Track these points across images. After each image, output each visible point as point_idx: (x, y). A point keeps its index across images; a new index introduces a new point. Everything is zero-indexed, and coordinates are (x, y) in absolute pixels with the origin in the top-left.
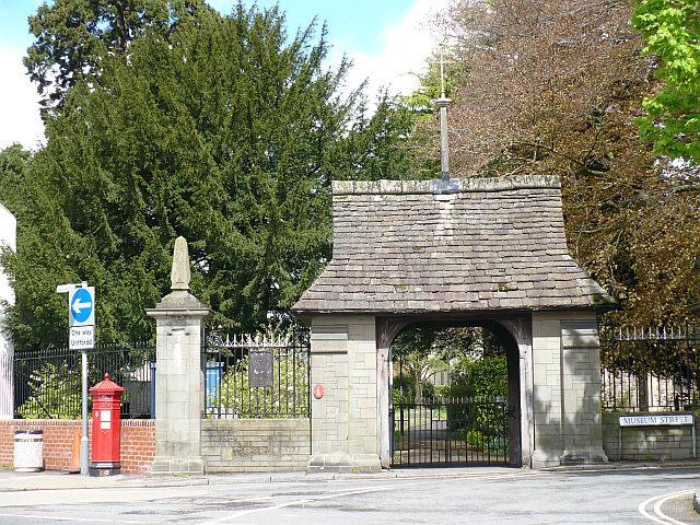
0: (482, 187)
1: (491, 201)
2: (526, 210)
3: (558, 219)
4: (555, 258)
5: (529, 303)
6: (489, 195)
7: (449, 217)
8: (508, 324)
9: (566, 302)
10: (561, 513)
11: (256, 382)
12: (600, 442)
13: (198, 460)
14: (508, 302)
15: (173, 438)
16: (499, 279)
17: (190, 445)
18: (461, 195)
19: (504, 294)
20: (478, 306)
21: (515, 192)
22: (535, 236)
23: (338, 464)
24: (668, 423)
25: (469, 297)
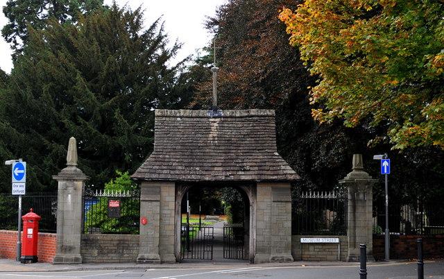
6: (237, 120)
8: (245, 188)
12: (290, 251)
14: (245, 177)
19: (243, 173)
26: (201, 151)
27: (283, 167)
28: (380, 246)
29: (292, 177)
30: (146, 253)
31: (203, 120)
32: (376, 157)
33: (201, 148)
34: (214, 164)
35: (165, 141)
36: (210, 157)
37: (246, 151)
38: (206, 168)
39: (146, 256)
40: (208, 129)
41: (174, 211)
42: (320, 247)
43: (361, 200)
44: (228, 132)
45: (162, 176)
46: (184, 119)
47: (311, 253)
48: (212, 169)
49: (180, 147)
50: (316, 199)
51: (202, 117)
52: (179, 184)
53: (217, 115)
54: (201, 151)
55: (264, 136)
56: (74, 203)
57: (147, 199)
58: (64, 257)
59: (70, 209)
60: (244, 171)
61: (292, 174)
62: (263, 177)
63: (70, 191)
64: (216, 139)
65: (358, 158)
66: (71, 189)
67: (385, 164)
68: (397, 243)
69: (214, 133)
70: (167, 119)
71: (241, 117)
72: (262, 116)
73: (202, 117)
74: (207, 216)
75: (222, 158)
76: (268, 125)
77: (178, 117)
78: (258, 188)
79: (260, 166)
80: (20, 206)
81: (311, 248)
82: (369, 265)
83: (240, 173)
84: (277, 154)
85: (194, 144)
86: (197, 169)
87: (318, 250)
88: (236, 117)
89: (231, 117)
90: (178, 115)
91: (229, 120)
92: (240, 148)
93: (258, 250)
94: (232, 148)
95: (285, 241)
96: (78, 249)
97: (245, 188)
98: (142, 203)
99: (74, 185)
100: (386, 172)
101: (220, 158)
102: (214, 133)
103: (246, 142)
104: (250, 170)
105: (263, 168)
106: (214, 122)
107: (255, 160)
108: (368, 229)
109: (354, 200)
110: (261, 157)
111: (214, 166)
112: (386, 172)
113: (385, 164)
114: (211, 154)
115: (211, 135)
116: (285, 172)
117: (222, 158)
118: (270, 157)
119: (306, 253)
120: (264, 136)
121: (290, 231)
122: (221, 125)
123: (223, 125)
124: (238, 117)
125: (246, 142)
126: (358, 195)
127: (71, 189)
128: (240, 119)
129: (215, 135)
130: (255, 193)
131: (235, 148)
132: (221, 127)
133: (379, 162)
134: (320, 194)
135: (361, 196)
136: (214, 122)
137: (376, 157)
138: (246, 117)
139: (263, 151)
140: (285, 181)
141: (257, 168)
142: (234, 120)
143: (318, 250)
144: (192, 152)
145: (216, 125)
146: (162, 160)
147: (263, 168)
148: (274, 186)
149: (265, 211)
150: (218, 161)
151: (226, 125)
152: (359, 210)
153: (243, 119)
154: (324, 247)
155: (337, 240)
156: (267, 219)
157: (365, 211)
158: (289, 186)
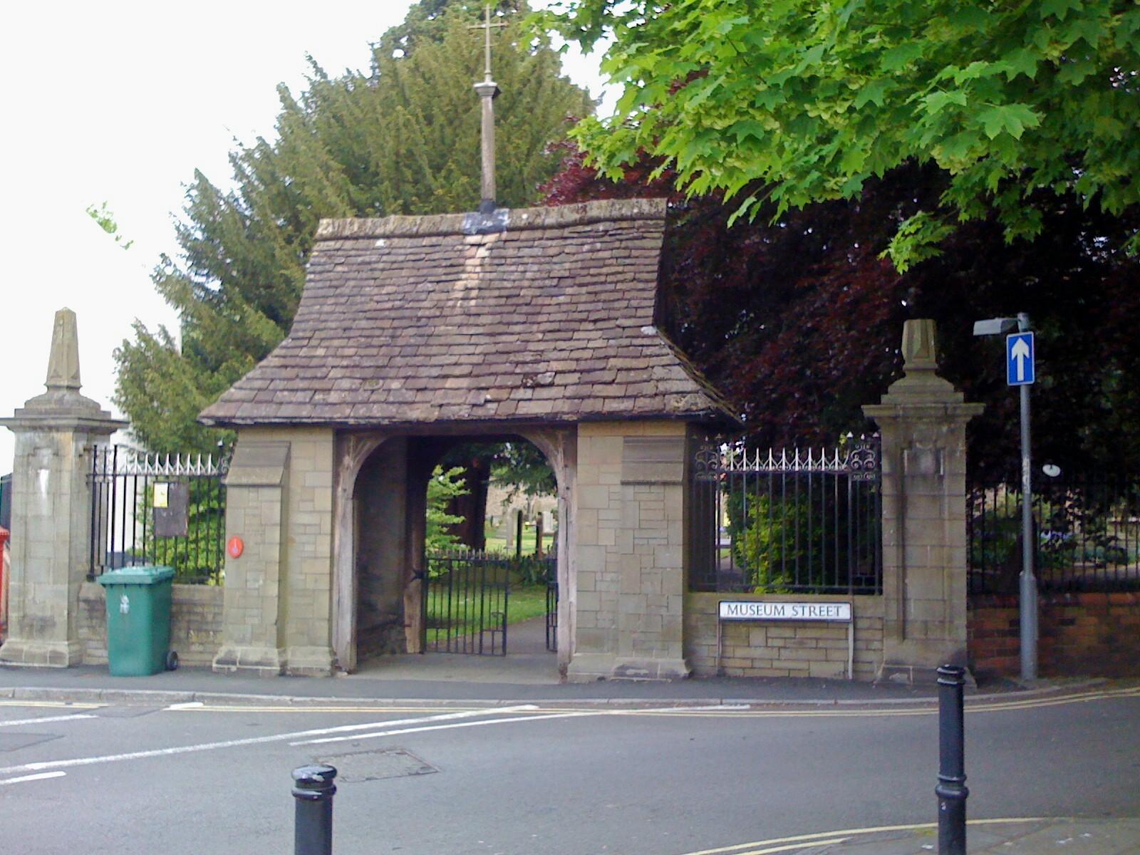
0: (539, 221)
1: (549, 243)
2: (601, 254)
3: (650, 268)
4: (628, 332)
5: (563, 407)
6: (549, 233)
7: (478, 269)
8: (540, 440)
9: (626, 405)
10: (376, 319)
11: (896, 146)
12: (678, 647)
13: (63, 647)
14: (536, 406)
15: (33, 611)
16: (527, 369)
17: (836, 132)
18: (505, 235)
19: (528, 393)
20: (480, 413)
21: (588, 228)
22: (603, 297)
23: (258, 664)
24: (807, 616)
25: (472, 398)
26: (422, 331)
27: (659, 372)
28: (1003, 634)
29: (682, 404)
30: (241, 641)
31: (449, 240)
32: (984, 327)
33: (423, 321)
34: (446, 371)
35: (326, 309)
36: (444, 350)
37: (556, 326)
38: (421, 383)
39: (239, 651)
40: (456, 267)
41: (328, 518)
42: (788, 633)
43: (924, 477)
44: (513, 272)
45: (287, 412)
46: (396, 241)
47: (757, 653)
48: (439, 383)
49: (364, 324)
50: (803, 475)
51: (446, 234)
52: (342, 433)
53: (490, 224)
54: (422, 331)
55: (620, 277)
56: (54, 493)
57: (244, 481)
58: (25, 648)
59: (45, 510)
60: (533, 387)
61: (683, 393)
62: (589, 406)
63: (45, 461)
64: (474, 293)
65: (917, 336)
66: (46, 455)
67: (1020, 350)
68: (1071, 622)
69: (470, 279)
70: (348, 244)
71: (562, 226)
72: (623, 219)
73: (446, 234)
74: (840, 702)
75: (479, 349)
76: (638, 243)
77: (377, 237)
78: (580, 440)
79: (589, 371)
80: (211, 746)
81: (757, 636)
82: (977, 707)
83: (521, 393)
84: (650, 330)
85: (407, 313)
86: (395, 385)
87: (780, 643)
88: (544, 228)
89: (531, 227)
90: (379, 231)
91: (524, 235)
92: (540, 318)
93: (590, 639)
94: (516, 318)
95: (663, 611)
96: (62, 628)
97: (540, 440)
98: (232, 494)
99: (52, 444)
100: (1021, 376)
101: (471, 349)
102: (470, 279)
103: (562, 299)
104: (551, 385)
105: (597, 376)
106: (479, 245)
107: (575, 355)
108: (951, 576)
109: (900, 479)
110: (599, 343)
111: (446, 377)
112: (1021, 376)
113: (1020, 350)
114: (449, 340)
115: (460, 285)
116: (662, 387)
117: (479, 349)
118: (626, 342)
119: (740, 652)
120: (620, 277)
121: (676, 580)
122: (496, 252)
123: (503, 253)
124: (551, 227)
125: (562, 299)
126: (914, 459)
127: (46, 455)
128: (556, 233)
129: (471, 284)
130: (572, 458)
131: (523, 318)
132: (497, 259)
133: (997, 346)
134: (790, 459)
135: (927, 463)
136: (479, 245)
137: (984, 327)
138: (575, 224)
139: (611, 324)
140: (658, 417)
141: (574, 378)
142: (538, 234)
143: (780, 643)
144: (402, 333)
145: (483, 252)
146: (304, 362)
147: (597, 376)
148: (631, 432)
149: (603, 515)
150: (463, 359)
151: (510, 252)
152: (919, 510)
153: (566, 232)
154: (801, 633)
155: (844, 612)
156: (607, 538)
157: (941, 511)
158: (680, 432)
